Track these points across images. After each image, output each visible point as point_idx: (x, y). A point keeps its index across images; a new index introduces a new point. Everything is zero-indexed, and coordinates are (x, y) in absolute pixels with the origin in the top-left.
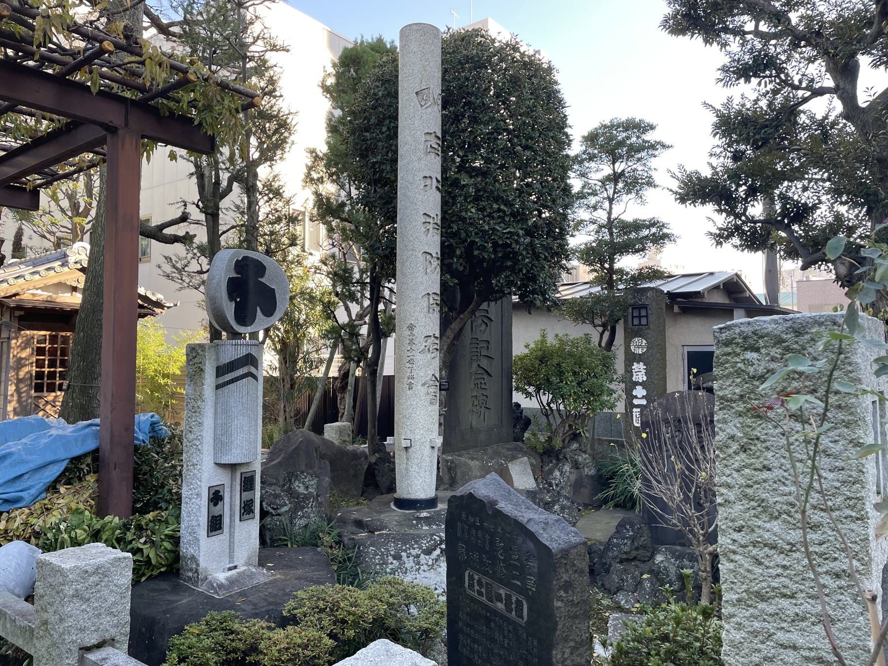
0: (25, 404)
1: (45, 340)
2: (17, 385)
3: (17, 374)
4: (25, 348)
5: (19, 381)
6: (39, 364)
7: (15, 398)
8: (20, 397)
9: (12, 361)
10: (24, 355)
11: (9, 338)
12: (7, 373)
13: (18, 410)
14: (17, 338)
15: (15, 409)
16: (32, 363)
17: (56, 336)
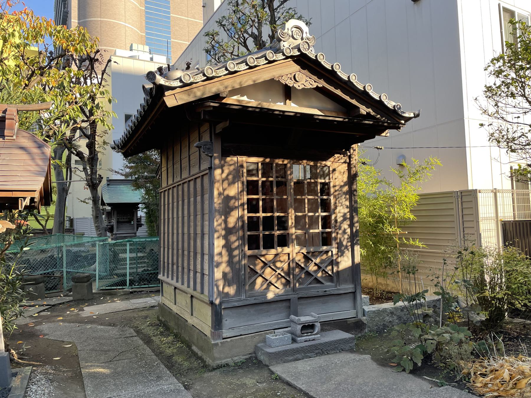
0: (237, 266)
1: (257, 170)
2: (226, 237)
3: (226, 221)
4: (233, 183)
5: (229, 231)
6: (252, 206)
7: (225, 258)
9: (217, 201)
10: (233, 191)
11: (210, 168)
12: (211, 221)
13: (230, 276)
14: (222, 167)
15: (225, 275)
16: (243, 205)
17: (270, 164)
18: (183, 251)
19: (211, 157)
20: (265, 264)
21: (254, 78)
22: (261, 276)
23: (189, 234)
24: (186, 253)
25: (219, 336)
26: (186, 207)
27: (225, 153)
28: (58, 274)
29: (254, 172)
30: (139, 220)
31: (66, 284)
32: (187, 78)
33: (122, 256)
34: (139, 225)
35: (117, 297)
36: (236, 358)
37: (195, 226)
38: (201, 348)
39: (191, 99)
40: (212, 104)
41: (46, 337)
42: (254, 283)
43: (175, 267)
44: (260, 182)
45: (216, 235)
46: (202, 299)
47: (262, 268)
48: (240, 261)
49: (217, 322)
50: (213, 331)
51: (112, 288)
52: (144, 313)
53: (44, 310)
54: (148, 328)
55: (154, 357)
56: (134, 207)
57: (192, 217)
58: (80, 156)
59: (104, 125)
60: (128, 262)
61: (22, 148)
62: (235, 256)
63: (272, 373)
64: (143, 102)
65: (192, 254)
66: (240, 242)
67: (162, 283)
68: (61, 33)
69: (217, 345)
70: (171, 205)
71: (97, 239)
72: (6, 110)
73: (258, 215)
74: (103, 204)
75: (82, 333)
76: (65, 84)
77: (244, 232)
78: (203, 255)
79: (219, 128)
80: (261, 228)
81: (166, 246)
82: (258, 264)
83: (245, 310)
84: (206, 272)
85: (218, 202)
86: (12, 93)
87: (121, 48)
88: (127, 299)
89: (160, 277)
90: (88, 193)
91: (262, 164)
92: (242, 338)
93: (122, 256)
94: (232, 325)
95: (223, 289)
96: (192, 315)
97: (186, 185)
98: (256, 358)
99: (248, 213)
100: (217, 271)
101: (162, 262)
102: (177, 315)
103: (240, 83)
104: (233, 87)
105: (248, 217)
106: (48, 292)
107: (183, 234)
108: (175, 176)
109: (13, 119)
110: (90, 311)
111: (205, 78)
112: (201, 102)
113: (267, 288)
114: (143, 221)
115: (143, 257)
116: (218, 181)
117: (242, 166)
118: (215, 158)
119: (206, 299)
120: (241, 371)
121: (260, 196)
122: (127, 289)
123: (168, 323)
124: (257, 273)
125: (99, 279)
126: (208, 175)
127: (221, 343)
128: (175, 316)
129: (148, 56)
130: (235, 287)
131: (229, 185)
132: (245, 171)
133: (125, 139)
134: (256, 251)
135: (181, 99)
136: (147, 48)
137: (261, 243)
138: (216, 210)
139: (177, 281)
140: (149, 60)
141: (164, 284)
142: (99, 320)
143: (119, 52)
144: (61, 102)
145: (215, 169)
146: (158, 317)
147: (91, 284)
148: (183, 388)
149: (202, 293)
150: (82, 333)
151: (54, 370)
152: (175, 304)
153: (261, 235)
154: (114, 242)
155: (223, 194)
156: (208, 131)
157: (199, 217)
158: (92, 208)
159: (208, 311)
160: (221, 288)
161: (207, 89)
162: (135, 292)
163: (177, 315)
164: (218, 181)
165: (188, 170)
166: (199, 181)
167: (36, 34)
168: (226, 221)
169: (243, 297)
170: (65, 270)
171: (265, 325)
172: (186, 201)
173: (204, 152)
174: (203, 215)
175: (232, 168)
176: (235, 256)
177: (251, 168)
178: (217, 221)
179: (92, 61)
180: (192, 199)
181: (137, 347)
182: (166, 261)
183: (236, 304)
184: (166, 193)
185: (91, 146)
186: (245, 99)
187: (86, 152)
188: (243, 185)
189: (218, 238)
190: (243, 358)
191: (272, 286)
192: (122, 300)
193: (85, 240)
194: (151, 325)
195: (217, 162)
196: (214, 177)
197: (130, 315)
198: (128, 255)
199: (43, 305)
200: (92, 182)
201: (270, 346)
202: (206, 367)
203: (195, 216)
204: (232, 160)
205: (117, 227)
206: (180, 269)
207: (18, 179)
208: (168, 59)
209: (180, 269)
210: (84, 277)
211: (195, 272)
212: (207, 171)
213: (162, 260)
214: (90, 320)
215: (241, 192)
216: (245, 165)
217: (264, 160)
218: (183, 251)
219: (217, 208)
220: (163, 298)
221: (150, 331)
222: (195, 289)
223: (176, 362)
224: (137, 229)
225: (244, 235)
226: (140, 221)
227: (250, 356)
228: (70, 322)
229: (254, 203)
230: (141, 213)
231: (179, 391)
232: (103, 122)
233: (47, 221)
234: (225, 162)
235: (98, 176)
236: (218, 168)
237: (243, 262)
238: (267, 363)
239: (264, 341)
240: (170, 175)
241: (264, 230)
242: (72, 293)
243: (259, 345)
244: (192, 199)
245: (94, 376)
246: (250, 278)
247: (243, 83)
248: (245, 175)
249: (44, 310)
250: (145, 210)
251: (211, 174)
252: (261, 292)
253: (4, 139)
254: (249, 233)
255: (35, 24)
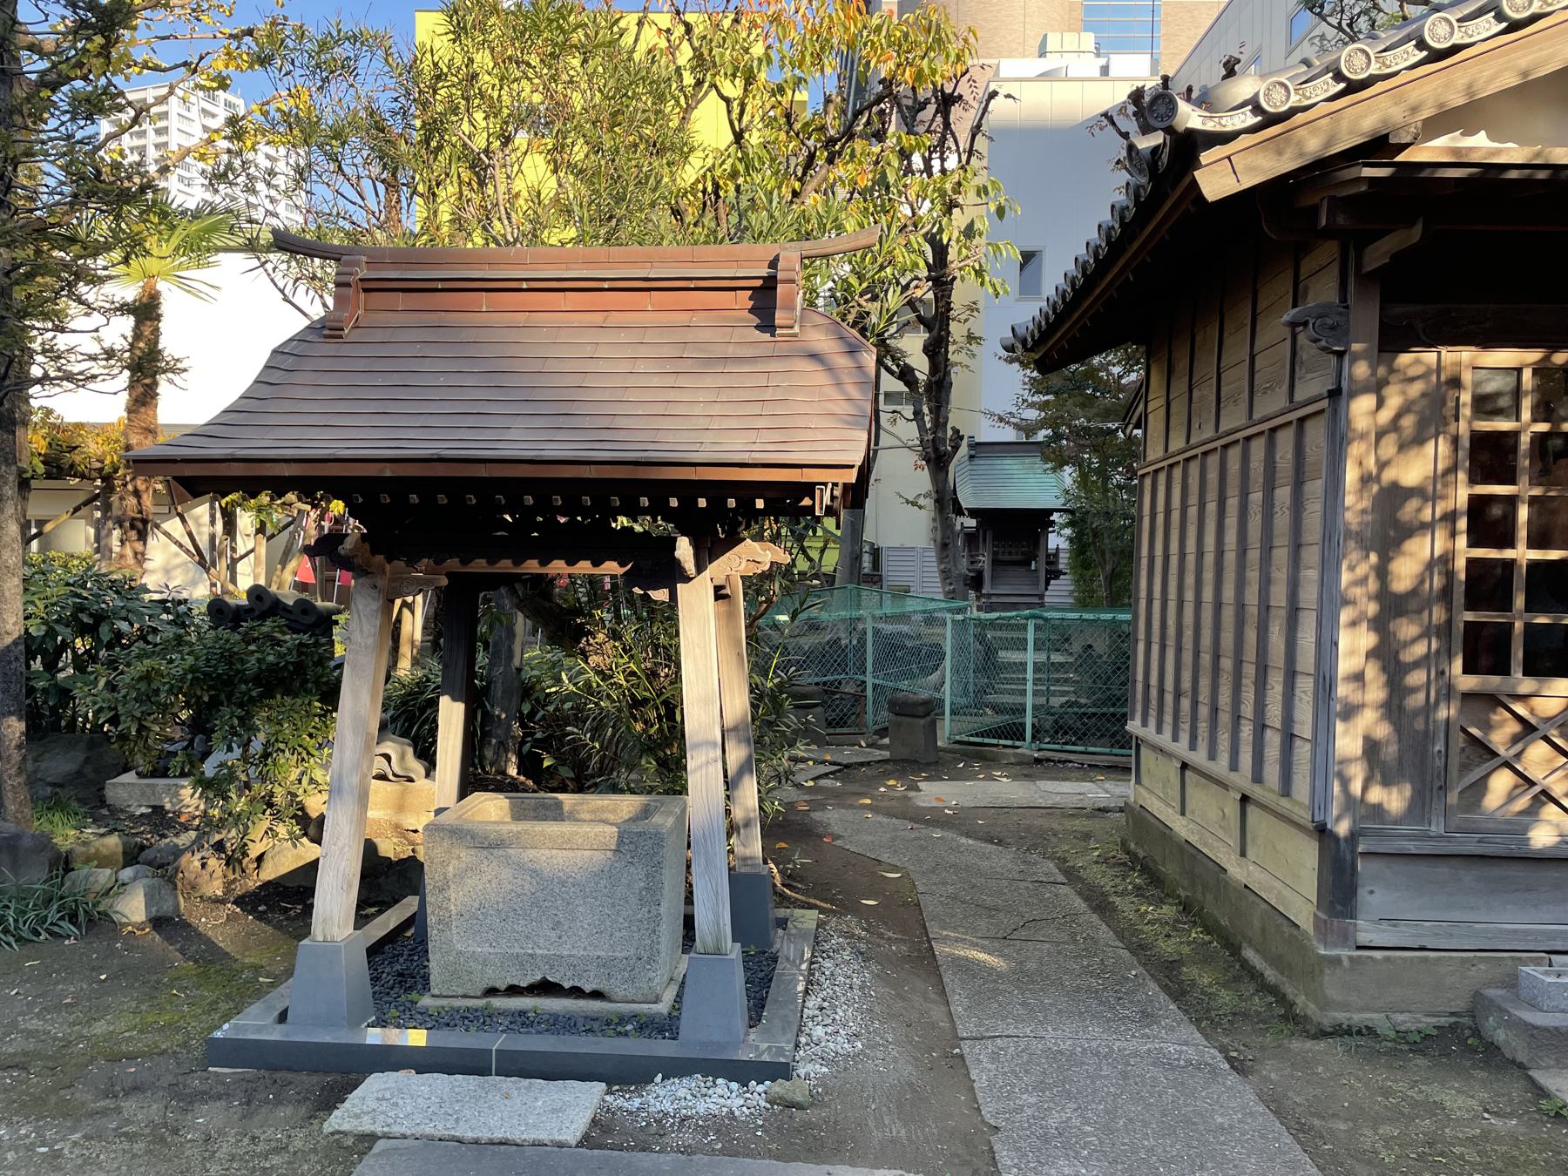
0: (1419, 724)
1: (1517, 393)
2: (1379, 624)
3: (1382, 572)
4: (1418, 440)
5: (1392, 606)
6: (1487, 523)
7: (1375, 692)
8: (1396, 689)
9: (1355, 503)
10: (1414, 470)
11: (1335, 394)
12: (1330, 568)
13: (1391, 751)
14: (1377, 387)
15: (1371, 747)
16: (1450, 517)
18: (1216, 657)
19: (1340, 355)
20: (1528, 729)
21: (1523, 63)
22: (1507, 765)
23: (1241, 606)
24: (1227, 664)
25: (1345, 938)
26: (1231, 521)
27: (1393, 340)
28: (849, 689)
29: (1504, 402)
30: (1052, 559)
31: (874, 715)
32: (1278, 94)
33: (1007, 656)
34: (1053, 574)
35: (999, 769)
36: (1400, 1018)
37: (1266, 582)
38: (1277, 962)
39: (1286, 164)
40: (1368, 172)
41: (838, 843)
42: (1481, 786)
43: (1186, 703)
44: (1525, 440)
45: (1345, 616)
46: (1285, 812)
47: (1516, 739)
48: (1429, 709)
49: (1339, 890)
50: (1322, 916)
51: (987, 741)
52: (1079, 824)
53: (826, 775)
54: (1095, 868)
55: (1125, 954)
56: (1038, 520)
57: (1254, 555)
58: (908, 377)
59: (982, 284)
60: (1030, 675)
61: (814, 356)
62: (1414, 690)
63: (1541, 1092)
64: (1121, 198)
65: (1250, 670)
66: (1434, 645)
67: (1138, 746)
68: (884, 33)
69: (1336, 961)
70: (1160, 518)
71: (943, 605)
72: (777, 259)
73: (1508, 554)
74: (959, 511)
75: (923, 848)
76: (891, 179)
77: (1449, 610)
78: (1291, 675)
79: (1377, 255)
80: (1519, 601)
81: (1156, 638)
82: (1502, 724)
83: (1443, 870)
84: (1304, 727)
85: (1360, 506)
86: (777, 214)
87: (1010, 54)
88: (1028, 777)
89: (1134, 726)
90: (923, 480)
91: (1535, 372)
92: (1426, 959)
93: (1007, 656)
94: (1388, 911)
95: (1365, 789)
96: (1243, 854)
97: (1234, 454)
98: (1476, 1032)
99: (1471, 544)
100: (1346, 732)
101: (1140, 687)
102: (1187, 847)
103: (1470, 86)
104: (1441, 105)
105: (1471, 562)
106: (831, 731)
107: (1218, 605)
108: (1195, 426)
109: (793, 281)
110: (934, 793)
111: (1342, 85)
112: (1321, 170)
113: (1533, 811)
114: (1063, 562)
115: (1061, 664)
116: (1363, 436)
117: (1455, 383)
118: (1355, 358)
119: (1304, 816)
120: (1421, 1061)
121: (1524, 488)
122: (1027, 749)
123: (1154, 864)
124: (1494, 754)
125: (953, 713)
126: (1326, 415)
127: (1350, 958)
128: (1181, 850)
129: (1092, 66)
130: (1407, 790)
131: (1402, 447)
132: (1466, 397)
133: (1047, 318)
134: (1495, 680)
135: (1251, 169)
136: (1088, 40)
137: (1518, 654)
138: (1348, 534)
139: (1193, 746)
140: (1097, 74)
141: (1143, 749)
142: (958, 821)
143: (1009, 67)
144: (889, 228)
145: (1353, 395)
146: (1124, 843)
147: (933, 723)
148: (1227, 1066)
149: (1286, 790)
150: (923, 848)
151: (864, 929)
152: (1183, 814)
153: (1518, 626)
154: (983, 615)
155: (1378, 479)
156: (1335, 269)
157: (1281, 555)
158: (934, 520)
159: (1307, 855)
160: (1356, 787)
161: (1345, 124)
162: (1048, 760)
163: (1187, 847)
164: (1363, 436)
165: (1244, 406)
166: (1286, 439)
167: (822, 48)
168: (1382, 572)
169: (1437, 828)
170: (870, 681)
171: (1515, 931)
172: (1233, 503)
173: (1315, 341)
174: (1297, 547)
175: (1416, 389)
176: (1414, 690)
177: (1490, 387)
178: (1352, 568)
179: (947, 102)
180: (1256, 497)
181: (1072, 916)
182: (1154, 681)
183: (1411, 847)
184: (1162, 477)
185: (936, 349)
186: (1479, 145)
187: (920, 364)
188: (1456, 450)
189: (1353, 624)
190: (1427, 1023)
191: (1552, 808)
192: (1015, 777)
193: (911, 605)
194: (1104, 860)
195: (1361, 370)
196: (1348, 422)
197: (1039, 822)
198: (1030, 657)
199: (823, 762)
200: (936, 450)
201: (1534, 1006)
202: (1293, 1020)
203: (1267, 549)
204: (1417, 361)
205: (993, 578)
206: (1204, 711)
207: (809, 435)
208: (1155, 63)
209: (1204, 711)
210: (916, 704)
211: (1261, 727)
212: (1324, 404)
213: (1140, 677)
214: (935, 818)
215: (1447, 472)
216: (1467, 377)
217: (1547, 358)
218: (1216, 657)
219: (1354, 527)
220: (1141, 789)
221: (1104, 879)
222: (1258, 778)
223: (1193, 984)
224: (1047, 584)
225: (1449, 622)
226: (1055, 563)
227: (1452, 1020)
228: (889, 814)
229: (1496, 511)
230: (1058, 540)
231: (1214, 1071)
232: (982, 277)
233: (822, 551)
234: (1392, 371)
235: (950, 433)
236: (1365, 389)
237: (1442, 713)
238: (1522, 1057)
239: (1512, 982)
240: (1178, 420)
241: (1529, 608)
242: (886, 741)
243: (1491, 993)
244: (1256, 497)
245: (967, 968)
246: (1465, 768)
247: (1478, 85)
248: (1466, 412)
249: (826, 775)
250: (1068, 531)
251: (1335, 412)
252: (1507, 822)
253: (773, 335)
254: (1469, 616)
255: (818, 20)
